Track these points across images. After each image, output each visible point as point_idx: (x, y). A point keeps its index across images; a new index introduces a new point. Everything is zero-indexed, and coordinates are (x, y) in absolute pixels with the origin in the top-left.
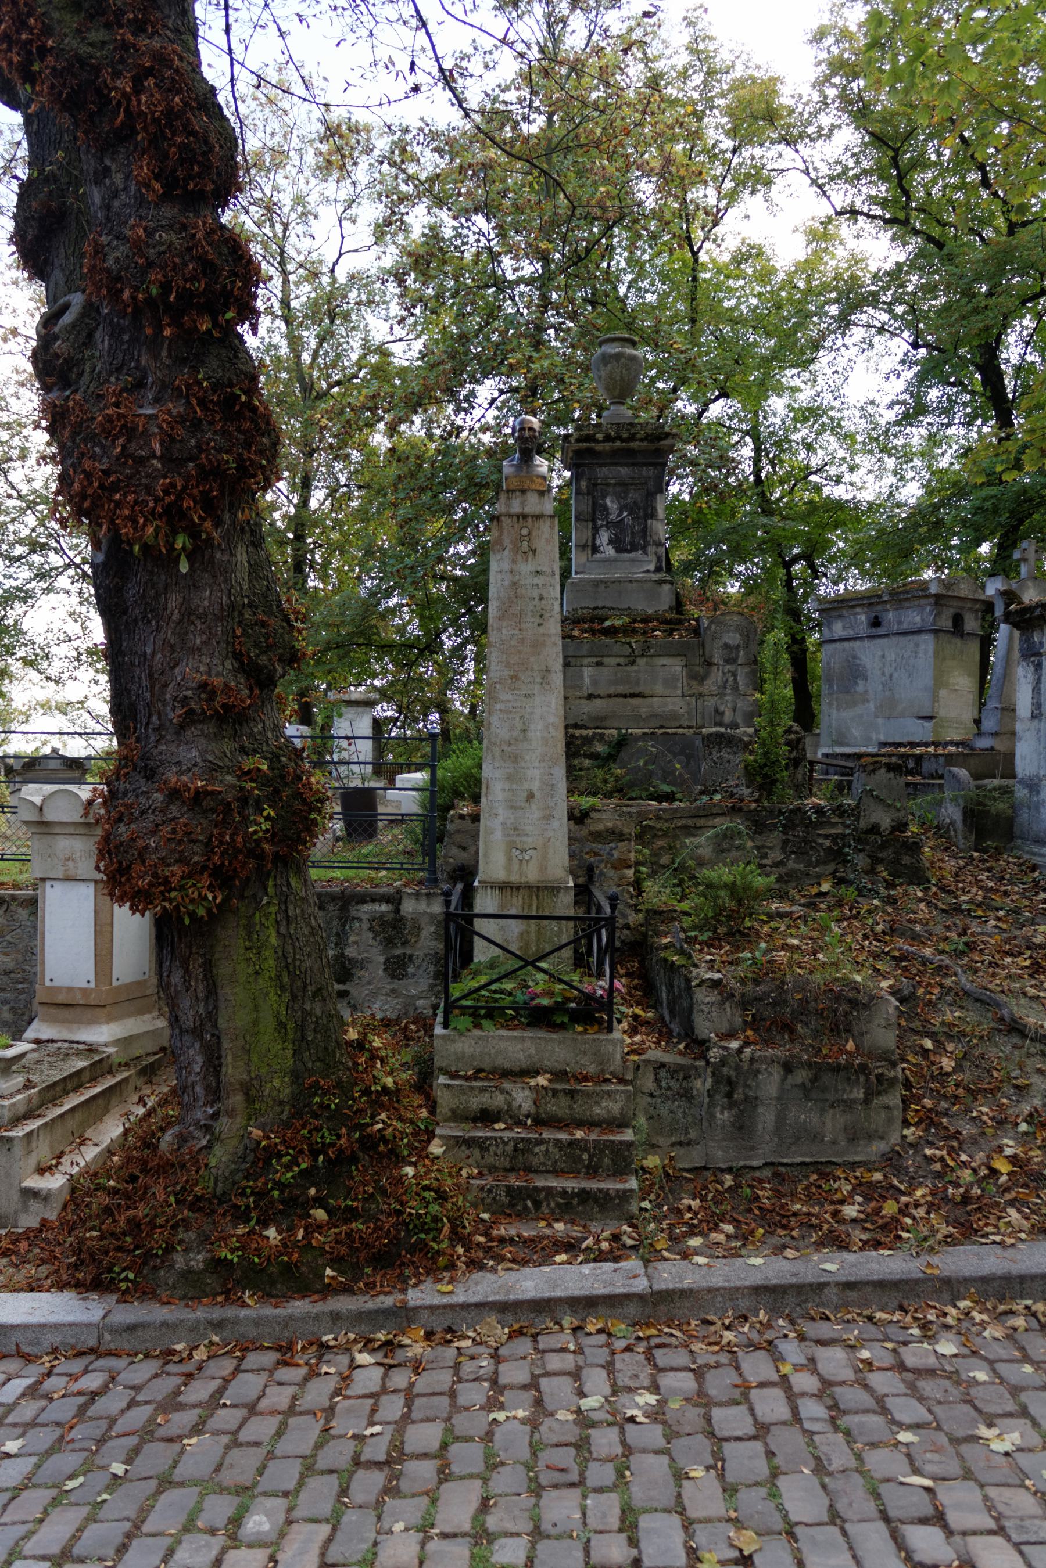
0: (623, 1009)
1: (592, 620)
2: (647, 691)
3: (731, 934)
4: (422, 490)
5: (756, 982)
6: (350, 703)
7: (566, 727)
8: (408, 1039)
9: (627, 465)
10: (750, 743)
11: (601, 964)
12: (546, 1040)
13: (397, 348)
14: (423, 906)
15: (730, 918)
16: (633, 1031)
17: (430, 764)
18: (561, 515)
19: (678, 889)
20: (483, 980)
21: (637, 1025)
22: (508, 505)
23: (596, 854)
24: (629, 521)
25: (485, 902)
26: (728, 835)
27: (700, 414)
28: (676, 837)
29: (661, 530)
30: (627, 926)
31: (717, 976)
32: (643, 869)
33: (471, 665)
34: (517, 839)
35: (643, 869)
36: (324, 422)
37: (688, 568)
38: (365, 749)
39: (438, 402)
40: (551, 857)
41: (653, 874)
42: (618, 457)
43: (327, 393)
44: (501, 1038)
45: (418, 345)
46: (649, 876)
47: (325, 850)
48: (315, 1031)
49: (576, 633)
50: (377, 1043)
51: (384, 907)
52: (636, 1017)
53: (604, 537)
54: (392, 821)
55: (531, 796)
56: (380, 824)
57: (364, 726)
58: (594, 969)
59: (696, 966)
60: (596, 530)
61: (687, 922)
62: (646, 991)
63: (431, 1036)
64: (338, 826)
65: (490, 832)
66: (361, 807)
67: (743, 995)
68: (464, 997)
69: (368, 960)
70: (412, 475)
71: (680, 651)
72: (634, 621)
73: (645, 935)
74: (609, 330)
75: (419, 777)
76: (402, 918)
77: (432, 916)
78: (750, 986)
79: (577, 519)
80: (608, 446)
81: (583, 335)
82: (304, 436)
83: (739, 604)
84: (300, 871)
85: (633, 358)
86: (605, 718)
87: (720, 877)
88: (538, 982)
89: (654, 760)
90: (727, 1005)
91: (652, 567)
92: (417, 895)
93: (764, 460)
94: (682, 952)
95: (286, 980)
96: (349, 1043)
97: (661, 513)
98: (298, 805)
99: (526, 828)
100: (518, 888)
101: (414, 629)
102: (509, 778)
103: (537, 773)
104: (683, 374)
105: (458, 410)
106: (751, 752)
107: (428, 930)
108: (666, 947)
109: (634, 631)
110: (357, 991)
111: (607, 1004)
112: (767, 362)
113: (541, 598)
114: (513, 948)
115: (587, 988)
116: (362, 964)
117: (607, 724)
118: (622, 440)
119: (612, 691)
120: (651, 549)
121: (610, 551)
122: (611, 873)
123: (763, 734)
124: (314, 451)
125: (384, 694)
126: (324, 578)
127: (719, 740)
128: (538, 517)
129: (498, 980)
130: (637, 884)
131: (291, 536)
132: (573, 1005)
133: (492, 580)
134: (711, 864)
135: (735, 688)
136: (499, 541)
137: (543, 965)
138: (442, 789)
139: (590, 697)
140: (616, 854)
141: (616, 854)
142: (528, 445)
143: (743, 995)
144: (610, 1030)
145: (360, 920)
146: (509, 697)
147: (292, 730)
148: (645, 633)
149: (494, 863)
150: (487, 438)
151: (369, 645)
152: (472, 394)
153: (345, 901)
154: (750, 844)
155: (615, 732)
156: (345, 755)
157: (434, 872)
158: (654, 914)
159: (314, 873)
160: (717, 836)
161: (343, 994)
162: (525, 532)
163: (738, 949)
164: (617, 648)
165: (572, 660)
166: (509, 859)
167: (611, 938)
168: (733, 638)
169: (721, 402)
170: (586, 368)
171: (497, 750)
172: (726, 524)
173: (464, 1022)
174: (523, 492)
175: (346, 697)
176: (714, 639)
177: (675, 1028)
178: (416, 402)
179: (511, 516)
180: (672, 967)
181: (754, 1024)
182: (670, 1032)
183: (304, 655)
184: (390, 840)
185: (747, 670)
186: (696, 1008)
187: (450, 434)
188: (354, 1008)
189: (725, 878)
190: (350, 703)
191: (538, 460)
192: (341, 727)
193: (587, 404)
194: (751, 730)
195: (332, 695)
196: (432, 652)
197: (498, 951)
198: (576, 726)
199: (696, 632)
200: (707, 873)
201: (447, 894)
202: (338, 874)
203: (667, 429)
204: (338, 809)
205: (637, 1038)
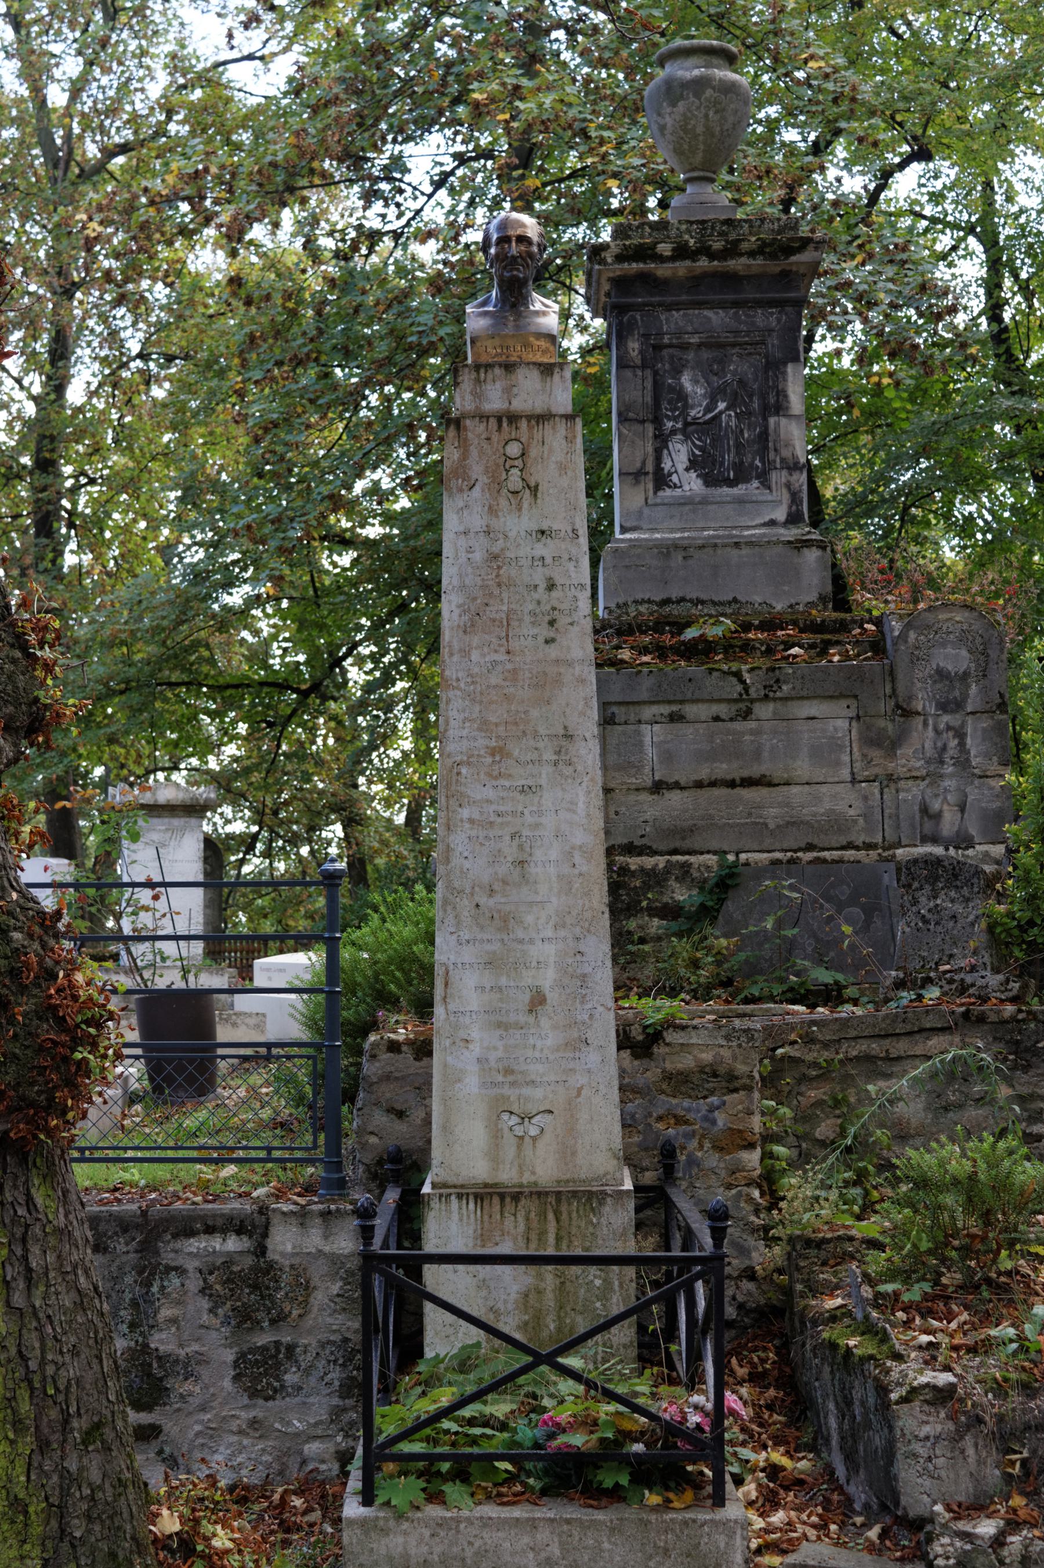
0: (746, 1453)
1: (658, 627)
2: (778, 773)
3: (970, 1286)
4: (298, 362)
5: (1028, 1389)
6: (155, 810)
7: (610, 851)
8: (287, 1528)
9: (722, 305)
10: (997, 877)
11: (695, 1356)
12: (586, 1526)
13: (238, 74)
14: (314, 1239)
15: (966, 1251)
16: (768, 1502)
17: (325, 935)
18: (587, 411)
19: (856, 1192)
20: (445, 1397)
21: (776, 1488)
22: (478, 395)
23: (680, 1121)
25: (446, 1229)
26: (958, 1074)
27: (874, 198)
28: (847, 1080)
29: (796, 437)
30: (749, 1274)
31: (945, 1378)
32: (780, 1150)
33: (405, 724)
34: (512, 1093)
35: (780, 1150)
36: (94, 228)
37: (858, 507)
38: (189, 908)
39: (328, 182)
40: (583, 1129)
41: (801, 1161)
42: (703, 290)
43: (100, 167)
44: (486, 1522)
45: (285, 67)
46: (793, 1165)
47: (106, 1123)
48: (89, 1518)
49: (625, 654)
50: (222, 1540)
51: (233, 1244)
52: (773, 1471)
54: (245, 1059)
55: (538, 1000)
56: (222, 1065)
57: (185, 858)
58: (681, 1367)
59: (898, 1357)
60: (662, 440)
61: (877, 1261)
62: (794, 1411)
63: (337, 1521)
64: (133, 1071)
65: (454, 1078)
66: (180, 1029)
67: (1001, 1418)
68: (405, 1435)
69: (202, 1359)
70: (278, 333)
71: (845, 689)
72: (746, 627)
73: (788, 1292)
74: (682, 26)
75: (301, 963)
76: (271, 1266)
77: (334, 1260)
78: (1016, 1399)
79: (623, 419)
80: (682, 268)
81: (624, 40)
82: (54, 255)
83: (962, 584)
84: (54, 1172)
85: (730, 89)
87: (942, 1164)
88: (563, 1400)
89: (796, 916)
90: (968, 1441)
91: (780, 514)
92: (302, 1216)
93: (1008, 282)
94: (868, 1329)
95: (25, 1407)
96: (162, 1543)
97: (796, 402)
98: (47, 1032)
99: (528, 1072)
100: (516, 1197)
101: (285, 656)
102: (491, 963)
103: (550, 951)
104: (834, 116)
105: (369, 197)
106: (1001, 897)
107: (327, 1290)
108: (833, 1317)
109: (747, 647)
110: (179, 1427)
111: (710, 1445)
112: (1008, 83)
113: (551, 586)
114: (508, 1326)
115: (668, 1411)
116: (188, 1368)
117: (697, 843)
118: (712, 256)
119: (704, 773)
120: (778, 477)
121: (693, 484)
122: (712, 1160)
123: (1025, 858)
124: (76, 286)
125: (227, 786)
126: (94, 544)
127: (933, 871)
128: (542, 418)
129: (478, 1396)
130: (768, 1181)
131: (26, 460)
132: (638, 1447)
133: (447, 550)
134: (923, 1136)
135: (963, 762)
136: (461, 470)
137: (573, 1361)
138: (352, 989)
139: (658, 787)
141: (721, 1119)
142: (516, 272)
143: (1001, 1418)
144: (719, 1500)
145: (181, 1271)
146: (490, 793)
147: (37, 869)
148: (769, 651)
149: (463, 1145)
150: (427, 252)
151: (193, 685)
152: (398, 163)
153: (149, 1232)
154: (1004, 1092)
155: (712, 859)
156: (145, 919)
157: (338, 1166)
158: (808, 1244)
159: (83, 1174)
160: (934, 1075)
161: (147, 1434)
162: (513, 449)
163: (988, 1318)
164: (712, 684)
165: (619, 712)
166: (496, 1135)
167: (716, 1298)
168: (955, 659)
169: (916, 168)
170: (629, 109)
171: (465, 904)
172: (930, 416)
173: (404, 1490)
174: (509, 367)
175: (147, 798)
176: (914, 660)
177: (859, 1492)
178: (283, 184)
179: (483, 417)
180: (847, 1362)
181: (1026, 1481)
182: (849, 1501)
183: (59, 716)
184: (242, 1097)
185: (985, 723)
186: (901, 1448)
187: (355, 248)
188: (172, 1462)
189: (953, 1166)
190: (155, 810)
191: (538, 302)
192: (137, 862)
193: (635, 182)
194: (998, 850)
195: (117, 794)
196: (325, 698)
197: (476, 1334)
198: (630, 849)
199: (878, 647)
200: (916, 1157)
201: (365, 1214)
202: (134, 1174)
203: (804, 231)
204: (133, 1036)
205: (778, 1518)
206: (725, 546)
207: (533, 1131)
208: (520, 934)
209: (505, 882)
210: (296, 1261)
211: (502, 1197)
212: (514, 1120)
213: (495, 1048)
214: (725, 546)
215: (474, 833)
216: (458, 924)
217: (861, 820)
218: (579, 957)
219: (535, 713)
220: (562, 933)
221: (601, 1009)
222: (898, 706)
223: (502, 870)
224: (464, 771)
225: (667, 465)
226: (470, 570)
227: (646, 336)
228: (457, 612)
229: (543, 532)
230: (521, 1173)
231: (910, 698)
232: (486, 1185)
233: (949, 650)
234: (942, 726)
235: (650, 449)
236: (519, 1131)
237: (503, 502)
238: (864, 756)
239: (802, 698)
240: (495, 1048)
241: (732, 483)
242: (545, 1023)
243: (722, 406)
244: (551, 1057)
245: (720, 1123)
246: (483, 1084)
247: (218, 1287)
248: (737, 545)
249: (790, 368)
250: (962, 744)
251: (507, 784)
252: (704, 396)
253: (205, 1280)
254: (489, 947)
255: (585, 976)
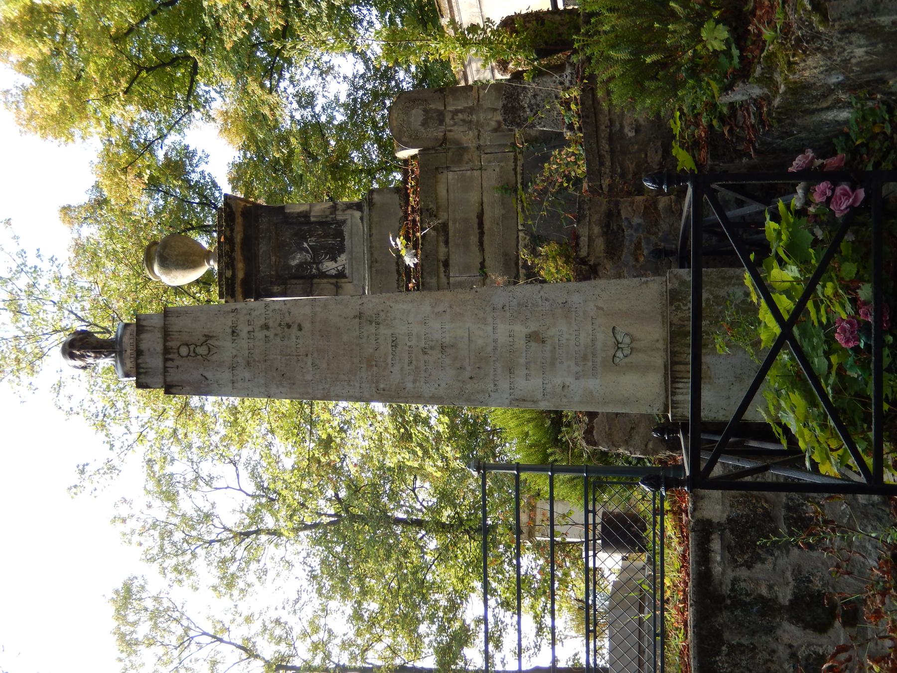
23: (638, 246)
24: (312, 241)
42: (250, 258)
51: (716, 545)
53: (329, 266)
55: (534, 337)
60: (323, 275)
69: (797, 571)
76: (730, 520)
80: (240, 266)
86: (506, 255)
91: (358, 214)
100: (673, 354)
103: (503, 329)
113: (266, 327)
119: (475, 249)
121: (343, 259)
135: (471, 110)
140: (636, 220)
145: (735, 581)
146: (396, 370)
162: (184, 351)
166: (631, 368)
179: (165, 370)
185: (450, 100)
206: (371, 242)
207: (627, 340)
208: (490, 349)
209: (455, 359)
210: (728, 503)
211: (674, 363)
212: (620, 354)
213: (569, 367)
214: (371, 242)
215: (422, 380)
216: (483, 391)
217: (502, 164)
218: (507, 308)
219: (345, 338)
220: (490, 320)
221: (542, 293)
222: (441, 145)
223: (448, 361)
224: (382, 386)
225: (334, 272)
226: (256, 380)
227: (272, 283)
228: (281, 389)
229: (233, 332)
230: (658, 349)
231: (436, 139)
232: (665, 376)
233: (412, 119)
234: (452, 122)
235: (325, 281)
236: (627, 351)
237: (215, 358)
238: (467, 163)
239: (437, 199)
240: (569, 367)
241: (343, 239)
242: (551, 333)
243: (305, 245)
244: (576, 328)
245: (640, 221)
246: (594, 376)
247: (746, 557)
248: (371, 236)
249: (287, 211)
250: (461, 111)
251: (391, 357)
252: (301, 254)
253: (742, 565)
254: (499, 371)
255: (519, 304)
